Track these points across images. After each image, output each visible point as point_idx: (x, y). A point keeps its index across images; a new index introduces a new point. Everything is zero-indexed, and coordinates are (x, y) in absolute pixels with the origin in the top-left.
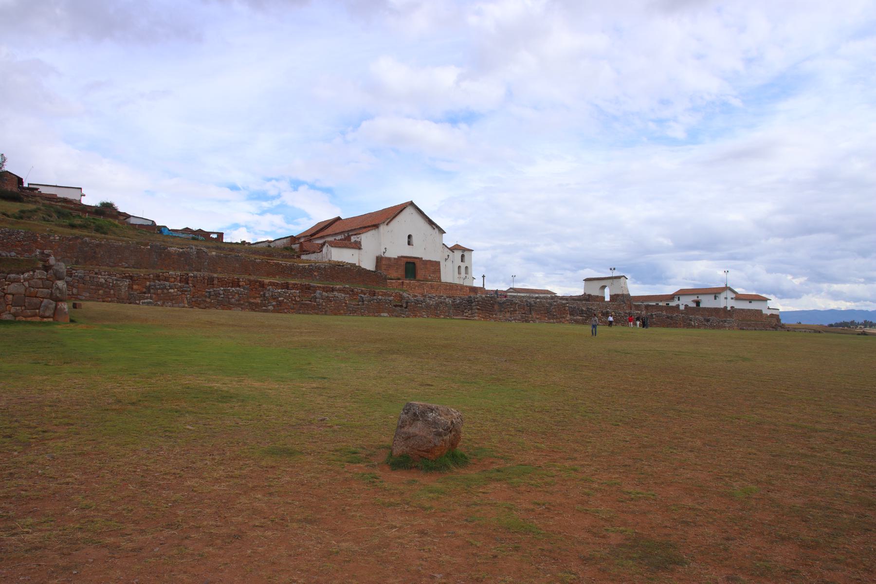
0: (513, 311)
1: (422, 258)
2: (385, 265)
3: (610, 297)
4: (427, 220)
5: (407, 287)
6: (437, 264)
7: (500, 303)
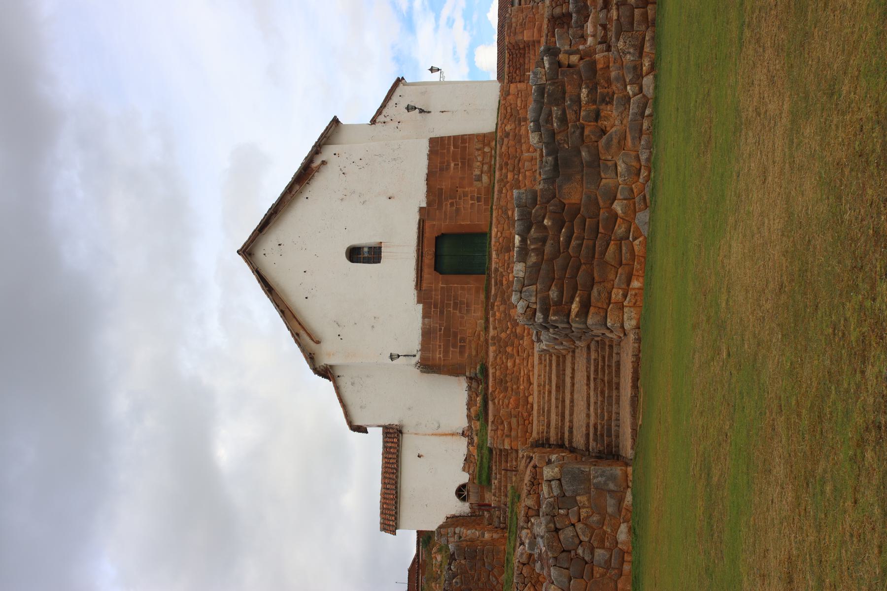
0: (592, 90)
1: (421, 209)
2: (446, 352)
3: (420, 303)
4: (297, 187)
5: (512, 356)
6: (438, 146)
7: (556, 166)
